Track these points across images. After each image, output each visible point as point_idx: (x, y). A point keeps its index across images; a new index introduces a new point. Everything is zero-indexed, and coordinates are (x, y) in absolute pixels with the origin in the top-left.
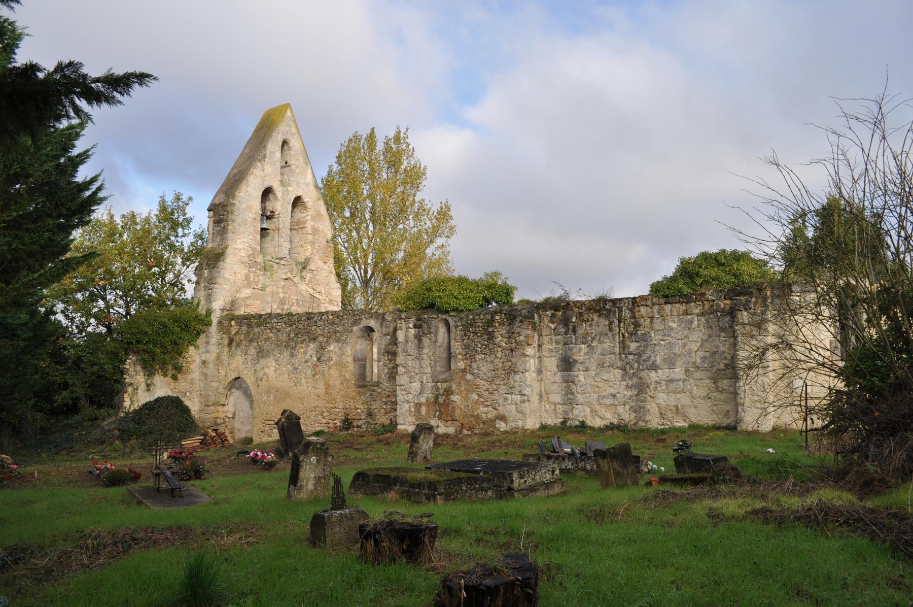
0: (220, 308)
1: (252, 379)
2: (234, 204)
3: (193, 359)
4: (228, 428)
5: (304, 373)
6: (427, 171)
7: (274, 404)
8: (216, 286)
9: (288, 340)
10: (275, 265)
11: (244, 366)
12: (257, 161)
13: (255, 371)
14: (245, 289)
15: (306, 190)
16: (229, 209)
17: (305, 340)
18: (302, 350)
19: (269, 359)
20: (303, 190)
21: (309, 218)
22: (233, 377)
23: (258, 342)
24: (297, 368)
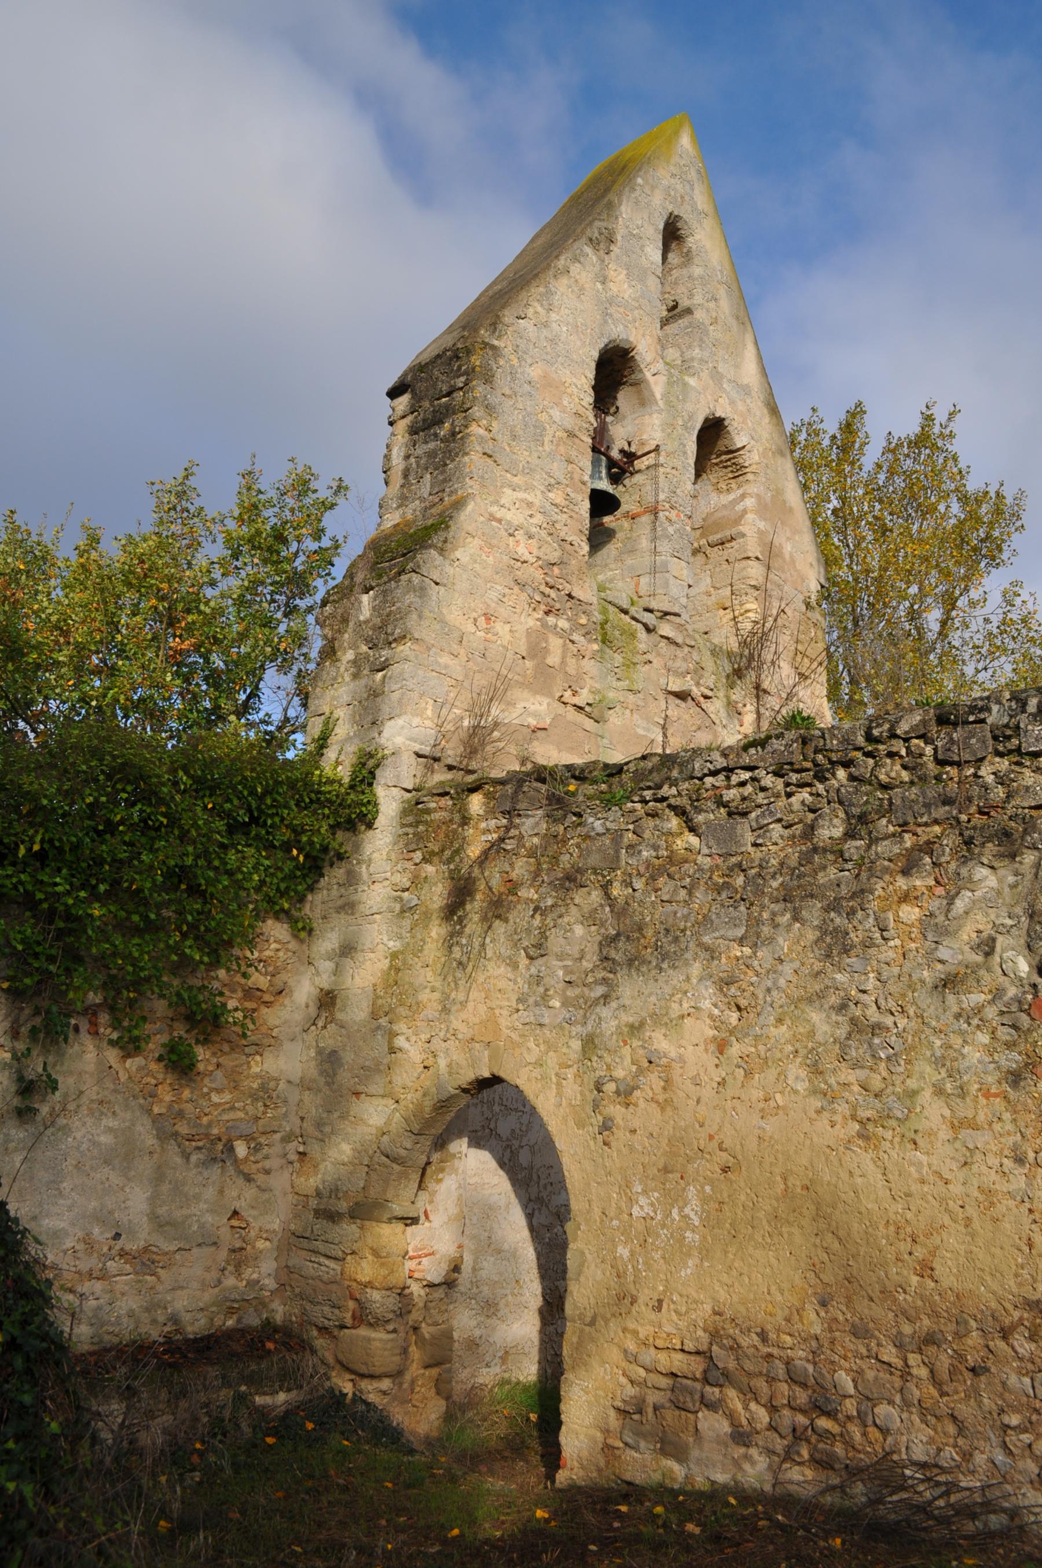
0: (417, 747)
1: (572, 1089)
2: (494, 348)
3: (279, 981)
4: (421, 1342)
5: (939, 1062)
6: (1028, 504)
7: (705, 1253)
8: (404, 649)
9: (806, 858)
10: (642, 634)
11: (525, 1016)
12: (584, 240)
13: (590, 1044)
14: (526, 694)
15: (741, 407)
16: (476, 360)
17: (928, 847)
18: (910, 913)
19: (676, 978)
20: (732, 402)
21: (749, 502)
22: (467, 1076)
23: (606, 887)
24: (876, 1028)
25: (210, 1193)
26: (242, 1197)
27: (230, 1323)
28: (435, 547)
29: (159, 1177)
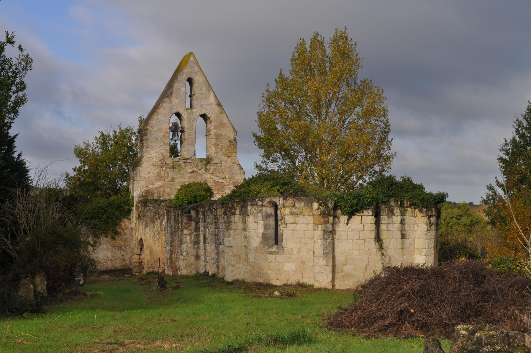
3: (126, 226)
14: (157, 182)
25: (119, 253)
26: (124, 253)
27: (123, 268)
28: (138, 166)
29: (112, 251)
